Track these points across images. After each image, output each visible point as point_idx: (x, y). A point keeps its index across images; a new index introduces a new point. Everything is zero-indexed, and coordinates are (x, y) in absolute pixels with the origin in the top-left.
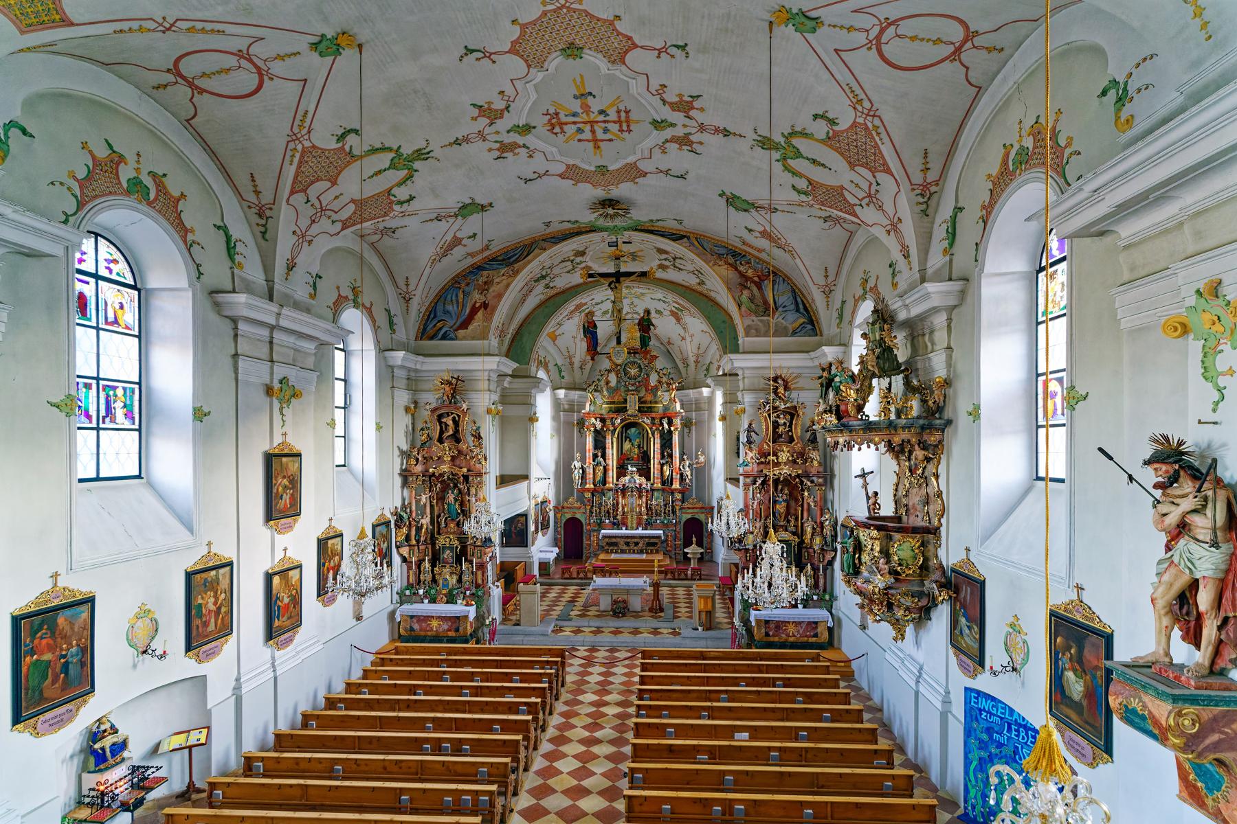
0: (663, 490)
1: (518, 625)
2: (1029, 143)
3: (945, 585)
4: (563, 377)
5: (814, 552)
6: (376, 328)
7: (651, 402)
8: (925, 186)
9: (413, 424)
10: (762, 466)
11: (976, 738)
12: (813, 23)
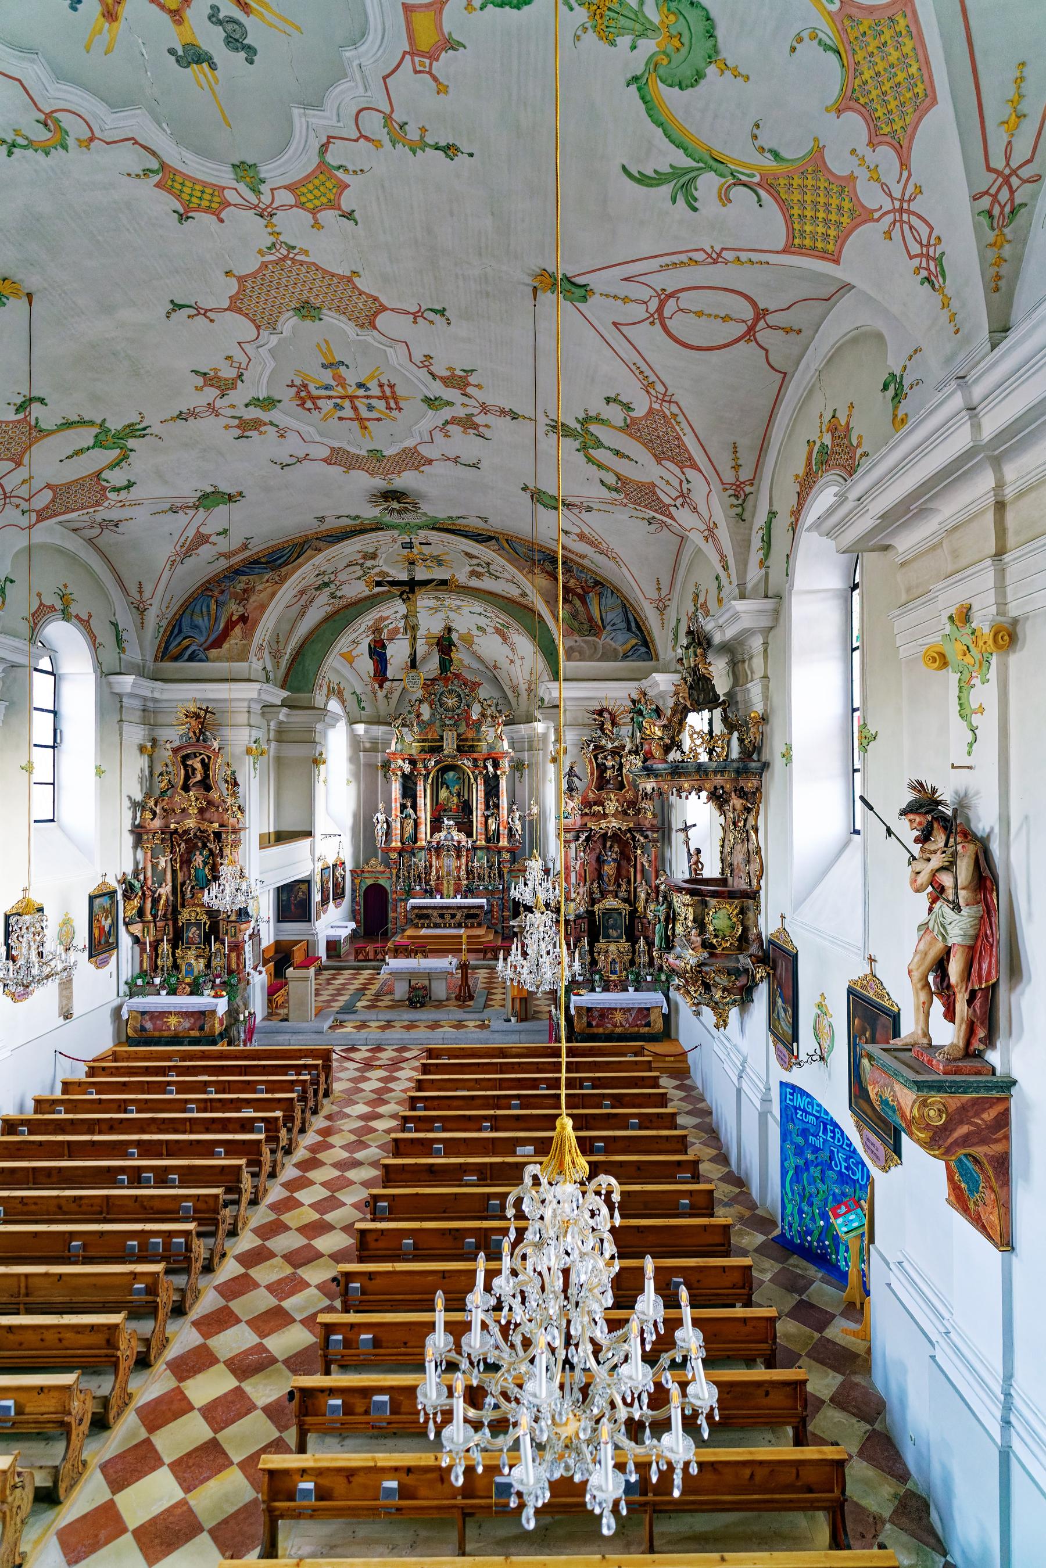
0: (488, 848)
1: (286, 1020)
2: (827, 440)
3: (764, 959)
4: (363, 709)
5: (649, 923)
6: (95, 645)
7: (473, 740)
8: (738, 486)
9: (151, 767)
10: (586, 818)
11: (793, 1143)
12: (582, 292)
